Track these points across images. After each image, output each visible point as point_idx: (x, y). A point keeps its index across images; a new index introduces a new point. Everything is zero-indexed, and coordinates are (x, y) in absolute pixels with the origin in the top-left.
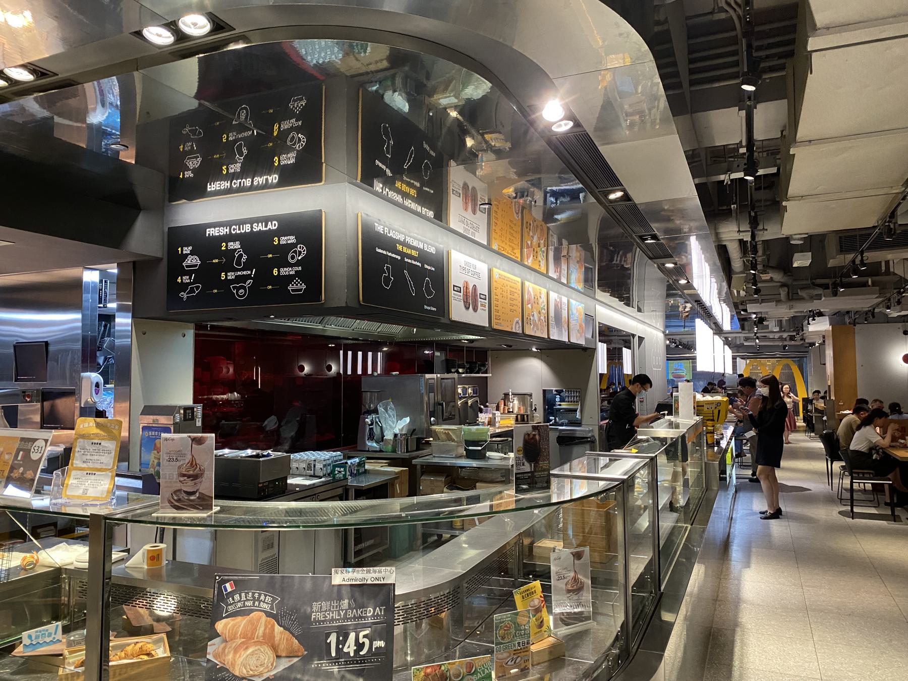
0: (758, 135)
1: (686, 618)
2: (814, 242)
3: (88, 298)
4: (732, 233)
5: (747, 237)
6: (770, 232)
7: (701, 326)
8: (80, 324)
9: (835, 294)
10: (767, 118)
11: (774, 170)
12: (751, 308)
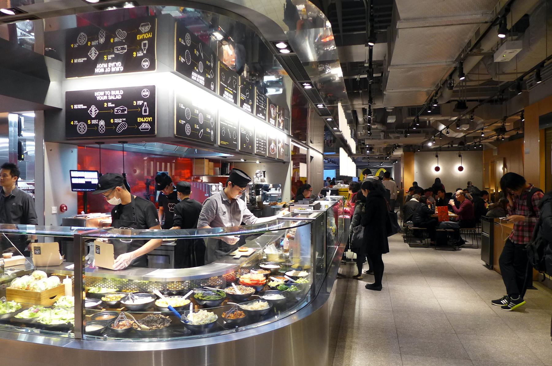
0: (374, 59)
1: (337, 291)
2: (397, 111)
3: (13, 130)
4: (359, 104)
5: (367, 107)
6: (378, 105)
7: (342, 152)
8: (8, 145)
9: (406, 136)
10: (378, 49)
11: (380, 75)
12: (367, 142)
